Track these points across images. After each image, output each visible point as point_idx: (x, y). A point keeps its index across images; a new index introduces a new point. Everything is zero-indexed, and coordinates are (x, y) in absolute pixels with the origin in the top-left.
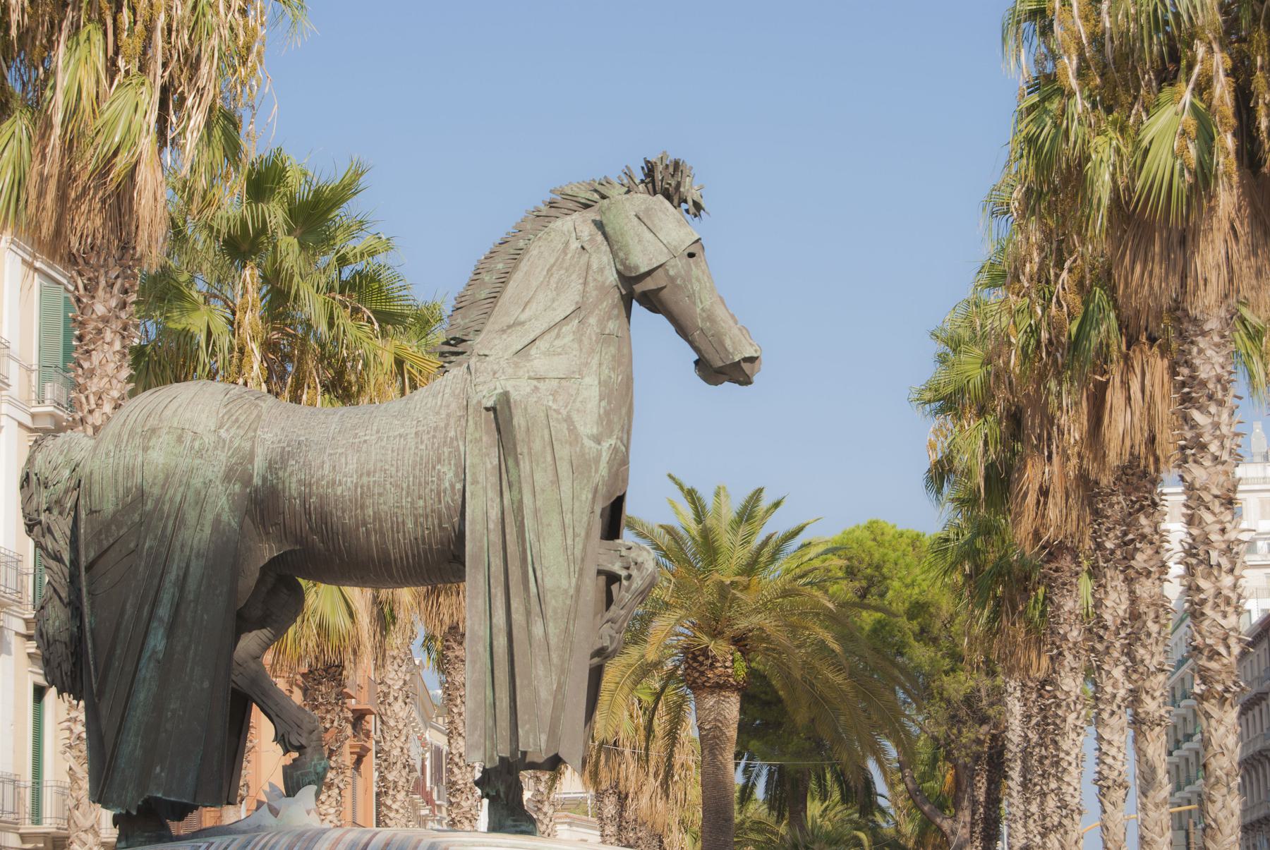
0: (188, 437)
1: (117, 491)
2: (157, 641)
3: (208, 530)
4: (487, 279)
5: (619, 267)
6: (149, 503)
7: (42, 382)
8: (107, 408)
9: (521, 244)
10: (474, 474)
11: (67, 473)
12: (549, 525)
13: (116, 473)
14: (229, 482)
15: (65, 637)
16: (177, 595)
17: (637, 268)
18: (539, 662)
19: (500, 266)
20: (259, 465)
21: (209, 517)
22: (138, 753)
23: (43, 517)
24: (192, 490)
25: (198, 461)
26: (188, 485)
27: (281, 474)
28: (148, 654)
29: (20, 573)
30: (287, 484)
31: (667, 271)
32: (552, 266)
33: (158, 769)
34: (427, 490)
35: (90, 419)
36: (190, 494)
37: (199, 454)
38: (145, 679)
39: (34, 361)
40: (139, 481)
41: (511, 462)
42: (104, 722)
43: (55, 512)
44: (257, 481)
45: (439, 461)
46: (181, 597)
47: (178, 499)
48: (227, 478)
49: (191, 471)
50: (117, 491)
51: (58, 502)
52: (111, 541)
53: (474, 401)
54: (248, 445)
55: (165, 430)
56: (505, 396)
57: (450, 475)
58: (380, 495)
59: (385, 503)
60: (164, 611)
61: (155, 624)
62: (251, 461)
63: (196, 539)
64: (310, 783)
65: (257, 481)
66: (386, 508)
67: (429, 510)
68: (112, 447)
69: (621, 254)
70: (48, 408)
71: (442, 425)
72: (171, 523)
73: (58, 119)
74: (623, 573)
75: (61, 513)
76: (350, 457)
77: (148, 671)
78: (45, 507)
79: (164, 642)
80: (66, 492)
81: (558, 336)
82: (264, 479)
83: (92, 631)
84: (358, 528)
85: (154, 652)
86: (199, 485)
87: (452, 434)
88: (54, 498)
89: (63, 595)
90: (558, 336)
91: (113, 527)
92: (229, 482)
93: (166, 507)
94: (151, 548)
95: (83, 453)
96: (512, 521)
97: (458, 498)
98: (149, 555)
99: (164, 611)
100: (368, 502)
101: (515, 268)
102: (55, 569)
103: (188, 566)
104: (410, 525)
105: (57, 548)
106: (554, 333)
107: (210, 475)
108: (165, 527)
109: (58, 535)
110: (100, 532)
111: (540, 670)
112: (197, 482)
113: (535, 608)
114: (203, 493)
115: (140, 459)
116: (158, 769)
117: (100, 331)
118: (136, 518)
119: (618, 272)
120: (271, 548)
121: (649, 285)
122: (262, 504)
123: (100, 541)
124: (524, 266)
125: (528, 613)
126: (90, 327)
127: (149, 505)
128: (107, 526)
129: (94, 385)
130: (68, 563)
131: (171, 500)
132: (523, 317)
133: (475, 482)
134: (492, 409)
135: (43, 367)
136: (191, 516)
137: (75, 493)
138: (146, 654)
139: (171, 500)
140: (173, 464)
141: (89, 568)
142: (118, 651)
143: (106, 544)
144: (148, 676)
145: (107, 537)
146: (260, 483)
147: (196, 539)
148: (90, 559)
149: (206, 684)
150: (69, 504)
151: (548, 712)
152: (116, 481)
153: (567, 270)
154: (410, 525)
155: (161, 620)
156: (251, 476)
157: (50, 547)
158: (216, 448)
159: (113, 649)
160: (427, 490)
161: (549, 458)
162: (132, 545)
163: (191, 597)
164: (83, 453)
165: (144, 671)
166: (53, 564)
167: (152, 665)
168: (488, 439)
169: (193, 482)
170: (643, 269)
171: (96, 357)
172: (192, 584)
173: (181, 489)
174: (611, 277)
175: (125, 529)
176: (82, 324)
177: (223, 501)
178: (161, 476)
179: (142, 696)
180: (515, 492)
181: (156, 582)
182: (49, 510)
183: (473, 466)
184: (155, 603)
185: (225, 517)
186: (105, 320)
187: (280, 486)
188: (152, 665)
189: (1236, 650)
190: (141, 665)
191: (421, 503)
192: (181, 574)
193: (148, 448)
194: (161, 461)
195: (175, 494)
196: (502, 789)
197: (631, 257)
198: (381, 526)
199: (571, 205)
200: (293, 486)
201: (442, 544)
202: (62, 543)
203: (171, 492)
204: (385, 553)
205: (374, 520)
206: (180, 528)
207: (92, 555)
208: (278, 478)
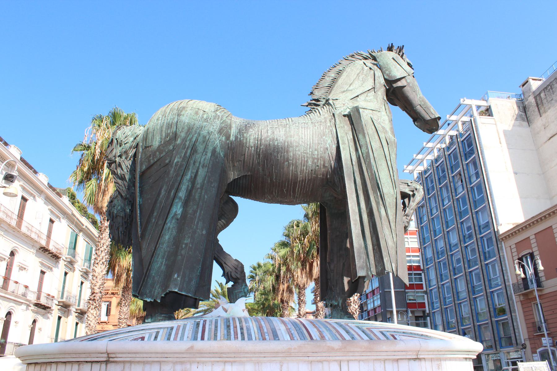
0: (201, 113)
1: (161, 135)
2: (177, 209)
3: (209, 155)
4: (328, 79)
5: (386, 77)
6: (179, 140)
7: (85, 262)
8: (105, 247)
9: (341, 69)
10: (343, 140)
11: (132, 139)
12: (381, 165)
13: (162, 127)
14: (221, 134)
15: (122, 214)
16: (190, 186)
17: (395, 76)
18: (385, 227)
19: (333, 75)
20: (233, 131)
21: (210, 148)
22: (163, 267)
23: (118, 159)
24: (201, 136)
25: (206, 123)
26: (199, 134)
27: (245, 135)
28: (172, 215)
29: (76, 300)
30: (248, 140)
31: (406, 81)
32: (359, 73)
33: (176, 276)
34: (319, 147)
35: (101, 249)
36: (201, 139)
37: (206, 120)
38: (169, 228)
39: (83, 259)
40: (174, 130)
41: (360, 136)
42: (144, 252)
43: (124, 157)
44: (232, 138)
45: (324, 135)
46: (193, 186)
47: (194, 139)
48: (220, 132)
49: (201, 128)
50: (161, 135)
51: (126, 152)
52: (156, 160)
53: (337, 113)
54: (229, 122)
55: (189, 109)
56: (357, 109)
57: (329, 141)
58: (297, 146)
59: (299, 151)
60: (182, 194)
61: (177, 200)
62: (230, 128)
63: (202, 160)
64: (242, 297)
65: (232, 138)
66: (299, 153)
67: (319, 156)
68: (161, 116)
69: (387, 72)
70: (85, 267)
71: (323, 121)
72: (189, 151)
73: (103, 179)
74: (411, 193)
75: (126, 158)
76: (281, 129)
77: (171, 224)
78: (119, 154)
79: (181, 210)
80: (130, 148)
81: (367, 96)
82: (236, 137)
83: (140, 205)
84: (284, 163)
85: (175, 214)
86: (205, 134)
87: (329, 124)
88: (124, 150)
89: (123, 195)
90: (367, 96)
91: (158, 153)
92: (221, 134)
93: (187, 143)
94: (178, 162)
95: (140, 132)
96: (363, 162)
97: (334, 147)
98: (176, 165)
99: (182, 194)
100: (291, 149)
101: (340, 77)
102: (121, 183)
103: (197, 172)
104: (310, 163)
105: (123, 173)
106: (366, 94)
107: (211, 130)
108: (186, 152)
109: (124, 167)
110: (150, 156)
111: (387, 231)
112: (204, 132)
113: (381, 202)
114: (207, 137)
115: (176, 120)
116: (176, 276)
117: (105, 229)
118: (171, 147)
119: (385, 79)
120: (234, 174)
121: (399, 84)
122: (234, 149)
123: (149, 161)
124: (344, 75)
125: (377, 203)
126: (103, 228)
127: (179, 141)
128: (154, 153)
129: (102, 241)
130: (127, 180)
131: (191, 140)
132: (350, 88)
133: (344, 143)
134: (349, 116)
135: (85, 260)
136: (200, 148)
137: (134, 150)
138: (171, 216)
139: (191, 140)
140: (193, 123)
141: (143, 174)
142: (155, 214)
143: (152, 162)
144: (171, 227)
145: (153, 159)
146: (234, 139)
147: (202, 160)
148: (142, 170)
149: (204, 232)
150: (131, 153)
151: (392, 252)
152: (162, 131)
153: (365, 75)
154: (310, 163)
155: (180, 198)
156: (230, 135)
157: (119, 172)
158: (215, 119)
159: (152, 212)
160: (319, 147)
161: (377, 137)
162: (167, 161)
163: (199, 186)
164: (140, 132)
165: (169, 224)
166: (120, 181)
167: (174, 221)
168: (348, 127)
169: (202, 132)
170: (398, 77)
171: (104, 235)
172: (199, 180)
173: (196, 135)
174: (383, 81)
175: (164, 153)
176: (101, 228)
177: (217, 142)
178: (186, 128)
179: (167, 237)
180: (364, 149)
181: (179, 179)
182: (120, 156)
183: (342, 137)
184: (178, 190)
185: (218, 150)
186: (107, 227)
187: (245, 141)
188: (174, 221)
189: (358, 313)
190: (168, 221)
191: (316, 152)
192: (193, 176)
193: (181, 115)
194: (187, 121)
195: (192, 138)
196: (341, 302)
197: (392, 73)
198: (296, 162)
199: (361, 58)
200: (251, 141)
201: (323, 175)
202: (125, 170)
203: (191, 136)
204: (296, 176)
205: (293, 159)
206: (193, 154)
207: (144, 167)
208: (243, 137)
